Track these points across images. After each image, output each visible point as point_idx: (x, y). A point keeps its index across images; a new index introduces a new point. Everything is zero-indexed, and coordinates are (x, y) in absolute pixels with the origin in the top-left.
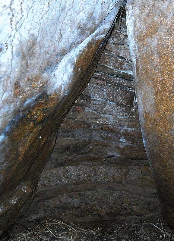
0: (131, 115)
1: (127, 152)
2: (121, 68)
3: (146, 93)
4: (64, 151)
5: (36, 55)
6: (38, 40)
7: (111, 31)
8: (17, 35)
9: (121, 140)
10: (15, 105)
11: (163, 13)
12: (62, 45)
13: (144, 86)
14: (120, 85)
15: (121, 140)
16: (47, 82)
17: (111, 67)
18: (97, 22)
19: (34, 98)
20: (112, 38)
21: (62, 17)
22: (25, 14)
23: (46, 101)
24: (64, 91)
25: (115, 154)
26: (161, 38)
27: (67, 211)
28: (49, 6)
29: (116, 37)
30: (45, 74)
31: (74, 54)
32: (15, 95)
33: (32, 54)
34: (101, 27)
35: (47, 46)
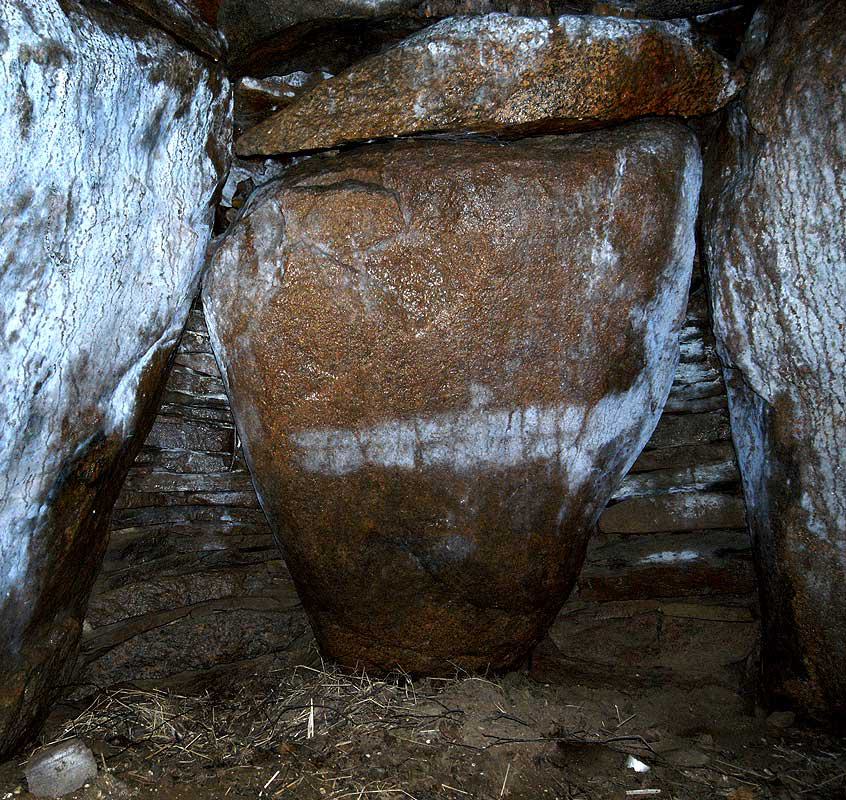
0: (233, 469)
1: (236, 540)
2: (206, 392)
3: (248, 413)
4: (122, 557)
5: (89, 378)
6: (90, 357)
7: (182, 337)
8: (67, 353)
9: (223, 518)
10: (63, 455)
11: (251, 304)
12: (120, 361)
13: (244, 403)
14: (207, 421)
15: (223, 518)
16: (104, 415)
17: (188, 393)
18: (164, 324)
19: (88, 441)
20: (184, 345)
21: (119, 323)
22: (77, 325)
23: (103, 447)
24: (126, 435)
25: (216, 547)
26: (254, 334)
27: (144, 669)
28: (103, 311)
29: (190, 342)
30: (100, 405)
31: (134, 373)
32: (64, 438)
33: (83, 377)
34: (170, 330)
35: (101, 364)
